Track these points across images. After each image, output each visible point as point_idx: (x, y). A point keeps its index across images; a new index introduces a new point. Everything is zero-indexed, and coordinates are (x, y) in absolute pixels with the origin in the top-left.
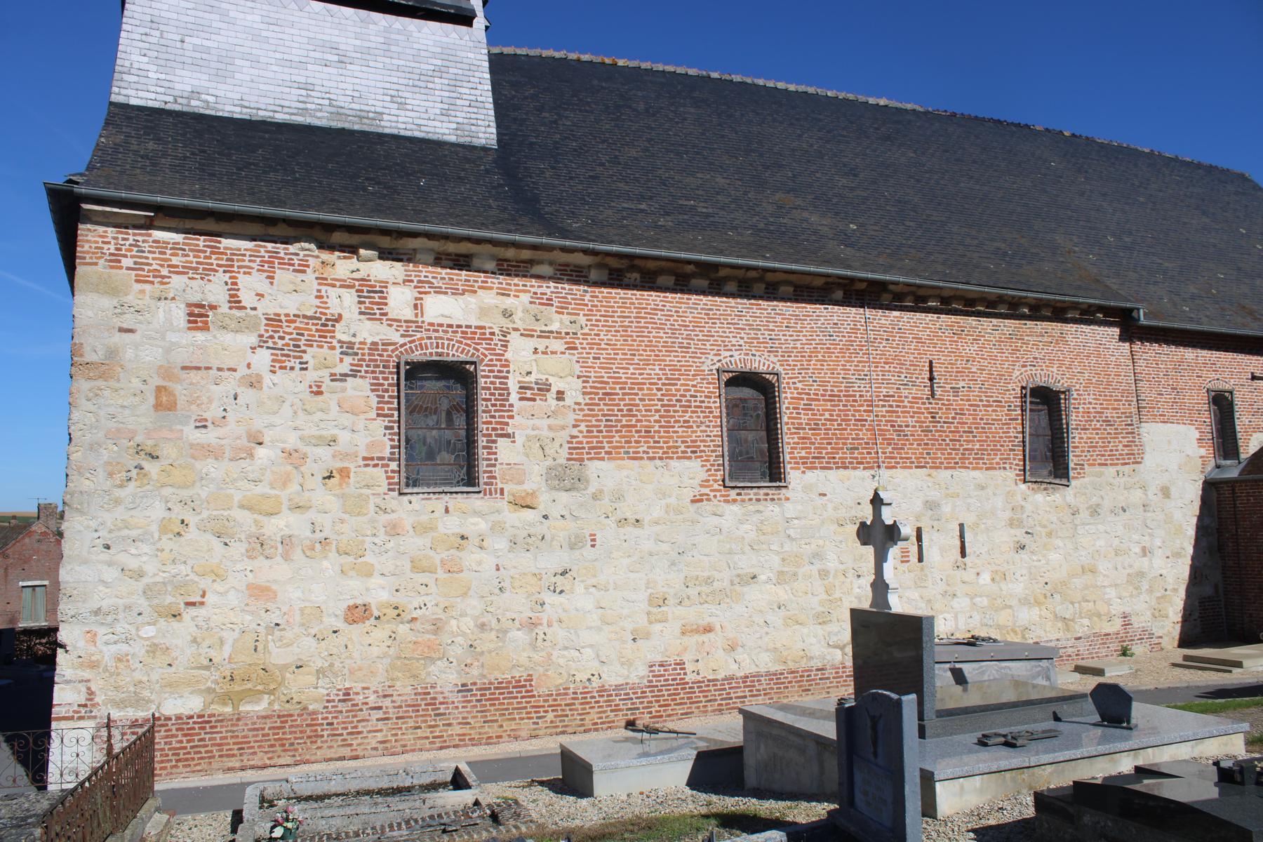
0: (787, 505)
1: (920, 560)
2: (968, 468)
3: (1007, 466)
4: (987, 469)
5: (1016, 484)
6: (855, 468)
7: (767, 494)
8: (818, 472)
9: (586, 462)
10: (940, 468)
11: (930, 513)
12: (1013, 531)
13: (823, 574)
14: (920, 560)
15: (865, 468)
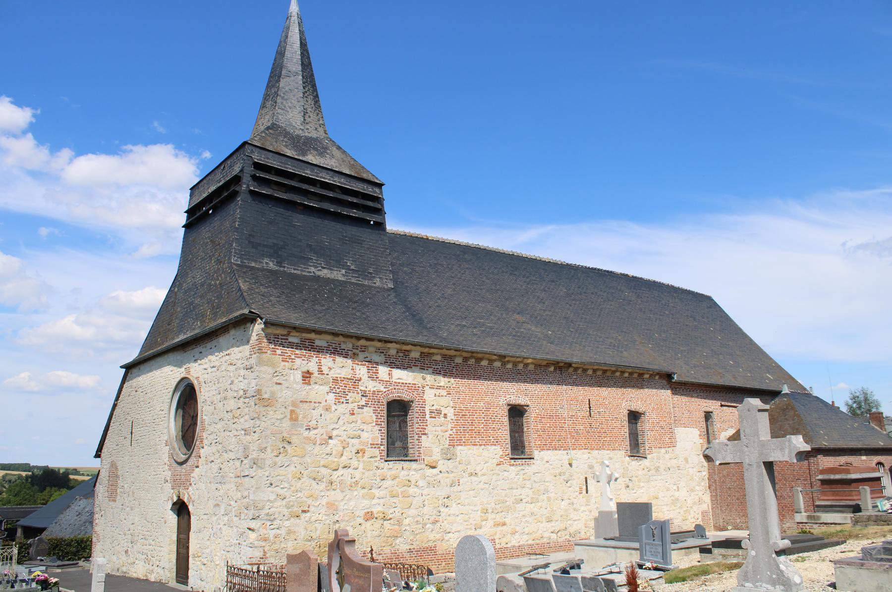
0: (533, 466)
1: (587, 493)
2: (605, 449)
3: (621, 448)
4: (613, 450)
5: (625, 457)
6: (560, 450)
7: (526, 462)
8: (545, 451)
9: (456, 447)
10: (594, 449)
11: (590, 470)
12: (624, 479)
13: (549, 499)
14: (587, 493)
15: (564, 450)
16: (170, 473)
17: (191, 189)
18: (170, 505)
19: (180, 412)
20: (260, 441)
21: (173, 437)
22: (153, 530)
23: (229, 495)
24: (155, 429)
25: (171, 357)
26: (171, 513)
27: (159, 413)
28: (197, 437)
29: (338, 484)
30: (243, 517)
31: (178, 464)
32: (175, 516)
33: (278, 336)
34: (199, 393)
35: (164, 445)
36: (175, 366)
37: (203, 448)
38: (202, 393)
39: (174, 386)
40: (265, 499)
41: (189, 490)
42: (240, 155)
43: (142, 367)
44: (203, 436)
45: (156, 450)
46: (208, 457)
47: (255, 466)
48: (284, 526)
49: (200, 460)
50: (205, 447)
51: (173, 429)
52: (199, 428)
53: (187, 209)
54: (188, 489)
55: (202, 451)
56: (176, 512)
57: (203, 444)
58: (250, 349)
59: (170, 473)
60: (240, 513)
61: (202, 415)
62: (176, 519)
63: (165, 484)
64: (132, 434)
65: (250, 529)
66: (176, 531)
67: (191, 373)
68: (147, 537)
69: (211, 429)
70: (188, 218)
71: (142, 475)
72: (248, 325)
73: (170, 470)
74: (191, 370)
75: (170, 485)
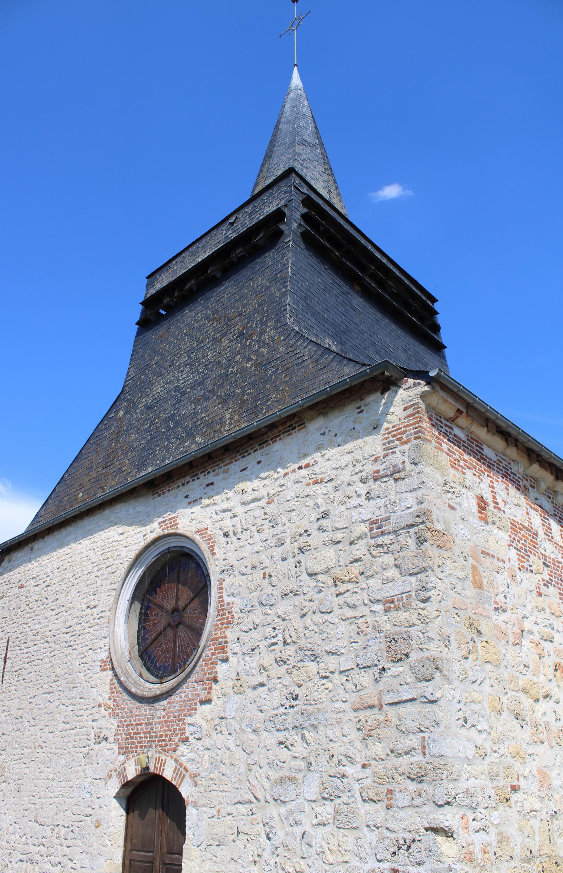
16: (115, 722)
17: (148, 278)
18: (115, 786)
19: (137, 606)
20: (439, 619)
21: (123, 653)
22: (57, 841)
23: (333, 752)
24: (71, 644)
25: (121, 509)
26: (115, 804)
27: (84, 613)
28: (207, 641)
29: (545, 731)
30: (401, 799)
31: (140, 702)
32: (123, 812)
33: (441, 417)
34: (210, 556)
35: (98, 669)
36: (131, 524)
37: (226, 660)
38: (217, 556)
39: (132, 555)
40: (460, 755)
41: (178, 753)
42: (283, 186)
43: (38, 545)
44: (225, 637)
45: (73, 681)
46: (243, 677)
47: (439, 674)
48: (493, 824)
49: (214, 686)
50: (233, 660)
51: (122, 638)
52: (213, 621)
53: (142, 300)
54: (175, 750)
55: (221, 669)
56: (124, 805)
57: (226, 652)
58: (384, 444)
59: (115, 722)
60: (390, 792)
61: (222, 597)
62: (124, 818)
63: (97, 746)
64: (5, 662)
65: (435, 830)
66: (122, 843)
67: (179, 526)
68: (37, 857)
69: (248, 621)
70: (144, 313)
71: (27, 733)
72: (371, 398)
73: (114, 716)
74: (178, 521)
75: (115, 747)
